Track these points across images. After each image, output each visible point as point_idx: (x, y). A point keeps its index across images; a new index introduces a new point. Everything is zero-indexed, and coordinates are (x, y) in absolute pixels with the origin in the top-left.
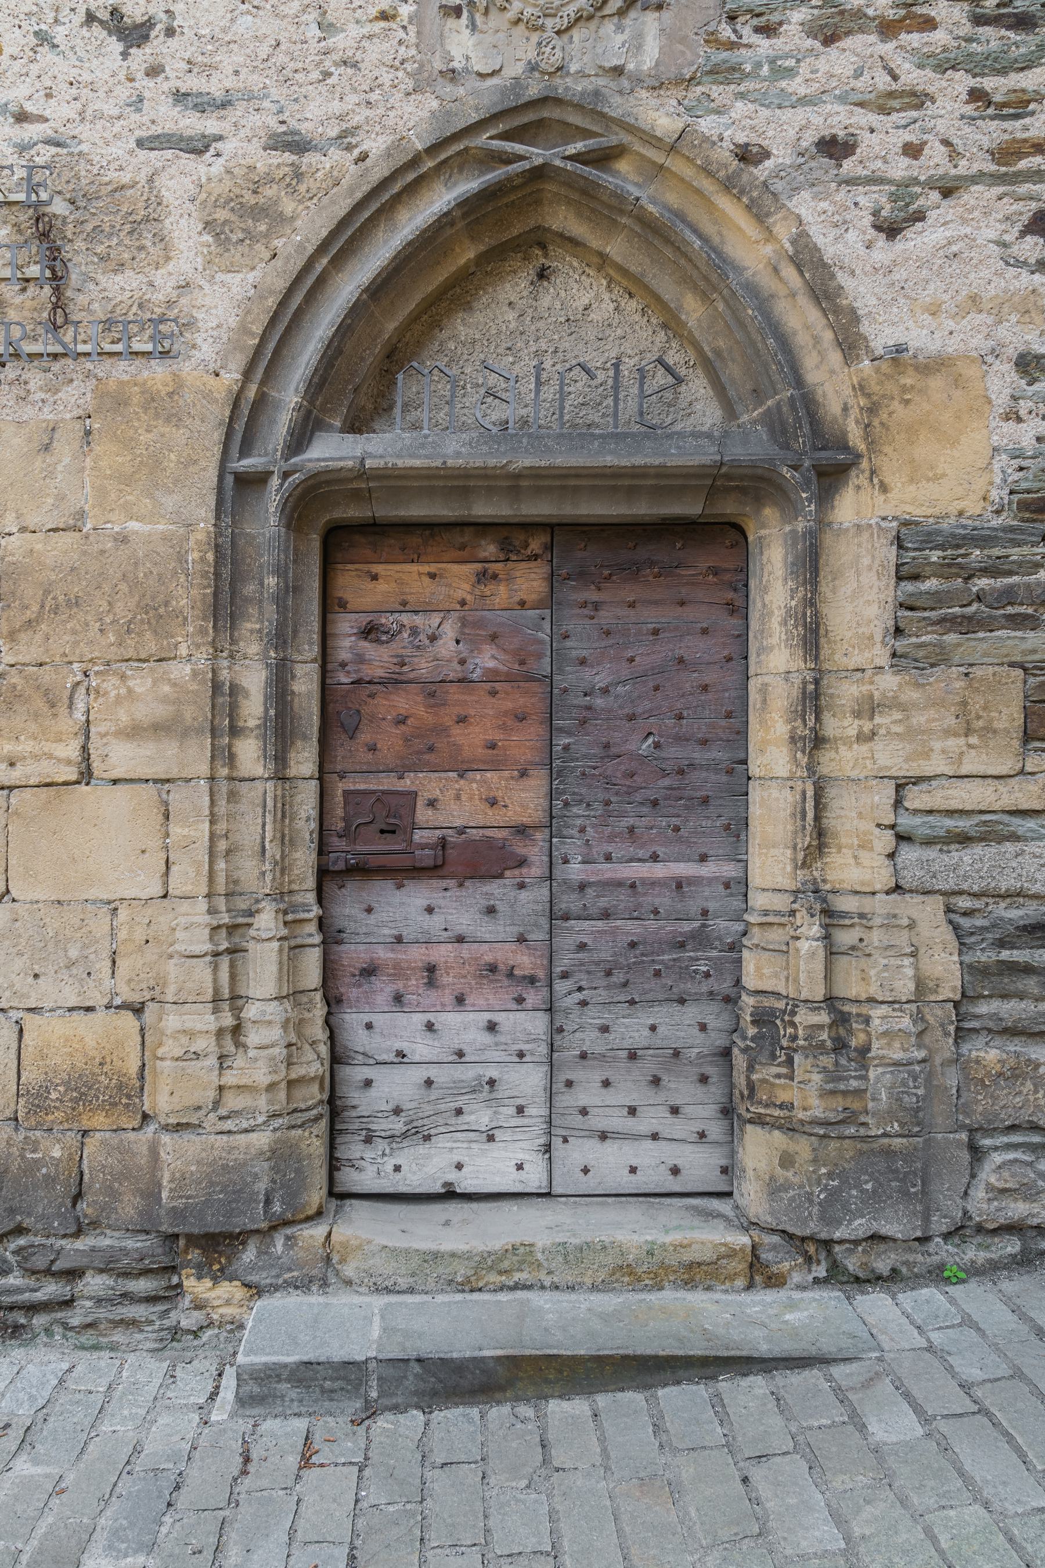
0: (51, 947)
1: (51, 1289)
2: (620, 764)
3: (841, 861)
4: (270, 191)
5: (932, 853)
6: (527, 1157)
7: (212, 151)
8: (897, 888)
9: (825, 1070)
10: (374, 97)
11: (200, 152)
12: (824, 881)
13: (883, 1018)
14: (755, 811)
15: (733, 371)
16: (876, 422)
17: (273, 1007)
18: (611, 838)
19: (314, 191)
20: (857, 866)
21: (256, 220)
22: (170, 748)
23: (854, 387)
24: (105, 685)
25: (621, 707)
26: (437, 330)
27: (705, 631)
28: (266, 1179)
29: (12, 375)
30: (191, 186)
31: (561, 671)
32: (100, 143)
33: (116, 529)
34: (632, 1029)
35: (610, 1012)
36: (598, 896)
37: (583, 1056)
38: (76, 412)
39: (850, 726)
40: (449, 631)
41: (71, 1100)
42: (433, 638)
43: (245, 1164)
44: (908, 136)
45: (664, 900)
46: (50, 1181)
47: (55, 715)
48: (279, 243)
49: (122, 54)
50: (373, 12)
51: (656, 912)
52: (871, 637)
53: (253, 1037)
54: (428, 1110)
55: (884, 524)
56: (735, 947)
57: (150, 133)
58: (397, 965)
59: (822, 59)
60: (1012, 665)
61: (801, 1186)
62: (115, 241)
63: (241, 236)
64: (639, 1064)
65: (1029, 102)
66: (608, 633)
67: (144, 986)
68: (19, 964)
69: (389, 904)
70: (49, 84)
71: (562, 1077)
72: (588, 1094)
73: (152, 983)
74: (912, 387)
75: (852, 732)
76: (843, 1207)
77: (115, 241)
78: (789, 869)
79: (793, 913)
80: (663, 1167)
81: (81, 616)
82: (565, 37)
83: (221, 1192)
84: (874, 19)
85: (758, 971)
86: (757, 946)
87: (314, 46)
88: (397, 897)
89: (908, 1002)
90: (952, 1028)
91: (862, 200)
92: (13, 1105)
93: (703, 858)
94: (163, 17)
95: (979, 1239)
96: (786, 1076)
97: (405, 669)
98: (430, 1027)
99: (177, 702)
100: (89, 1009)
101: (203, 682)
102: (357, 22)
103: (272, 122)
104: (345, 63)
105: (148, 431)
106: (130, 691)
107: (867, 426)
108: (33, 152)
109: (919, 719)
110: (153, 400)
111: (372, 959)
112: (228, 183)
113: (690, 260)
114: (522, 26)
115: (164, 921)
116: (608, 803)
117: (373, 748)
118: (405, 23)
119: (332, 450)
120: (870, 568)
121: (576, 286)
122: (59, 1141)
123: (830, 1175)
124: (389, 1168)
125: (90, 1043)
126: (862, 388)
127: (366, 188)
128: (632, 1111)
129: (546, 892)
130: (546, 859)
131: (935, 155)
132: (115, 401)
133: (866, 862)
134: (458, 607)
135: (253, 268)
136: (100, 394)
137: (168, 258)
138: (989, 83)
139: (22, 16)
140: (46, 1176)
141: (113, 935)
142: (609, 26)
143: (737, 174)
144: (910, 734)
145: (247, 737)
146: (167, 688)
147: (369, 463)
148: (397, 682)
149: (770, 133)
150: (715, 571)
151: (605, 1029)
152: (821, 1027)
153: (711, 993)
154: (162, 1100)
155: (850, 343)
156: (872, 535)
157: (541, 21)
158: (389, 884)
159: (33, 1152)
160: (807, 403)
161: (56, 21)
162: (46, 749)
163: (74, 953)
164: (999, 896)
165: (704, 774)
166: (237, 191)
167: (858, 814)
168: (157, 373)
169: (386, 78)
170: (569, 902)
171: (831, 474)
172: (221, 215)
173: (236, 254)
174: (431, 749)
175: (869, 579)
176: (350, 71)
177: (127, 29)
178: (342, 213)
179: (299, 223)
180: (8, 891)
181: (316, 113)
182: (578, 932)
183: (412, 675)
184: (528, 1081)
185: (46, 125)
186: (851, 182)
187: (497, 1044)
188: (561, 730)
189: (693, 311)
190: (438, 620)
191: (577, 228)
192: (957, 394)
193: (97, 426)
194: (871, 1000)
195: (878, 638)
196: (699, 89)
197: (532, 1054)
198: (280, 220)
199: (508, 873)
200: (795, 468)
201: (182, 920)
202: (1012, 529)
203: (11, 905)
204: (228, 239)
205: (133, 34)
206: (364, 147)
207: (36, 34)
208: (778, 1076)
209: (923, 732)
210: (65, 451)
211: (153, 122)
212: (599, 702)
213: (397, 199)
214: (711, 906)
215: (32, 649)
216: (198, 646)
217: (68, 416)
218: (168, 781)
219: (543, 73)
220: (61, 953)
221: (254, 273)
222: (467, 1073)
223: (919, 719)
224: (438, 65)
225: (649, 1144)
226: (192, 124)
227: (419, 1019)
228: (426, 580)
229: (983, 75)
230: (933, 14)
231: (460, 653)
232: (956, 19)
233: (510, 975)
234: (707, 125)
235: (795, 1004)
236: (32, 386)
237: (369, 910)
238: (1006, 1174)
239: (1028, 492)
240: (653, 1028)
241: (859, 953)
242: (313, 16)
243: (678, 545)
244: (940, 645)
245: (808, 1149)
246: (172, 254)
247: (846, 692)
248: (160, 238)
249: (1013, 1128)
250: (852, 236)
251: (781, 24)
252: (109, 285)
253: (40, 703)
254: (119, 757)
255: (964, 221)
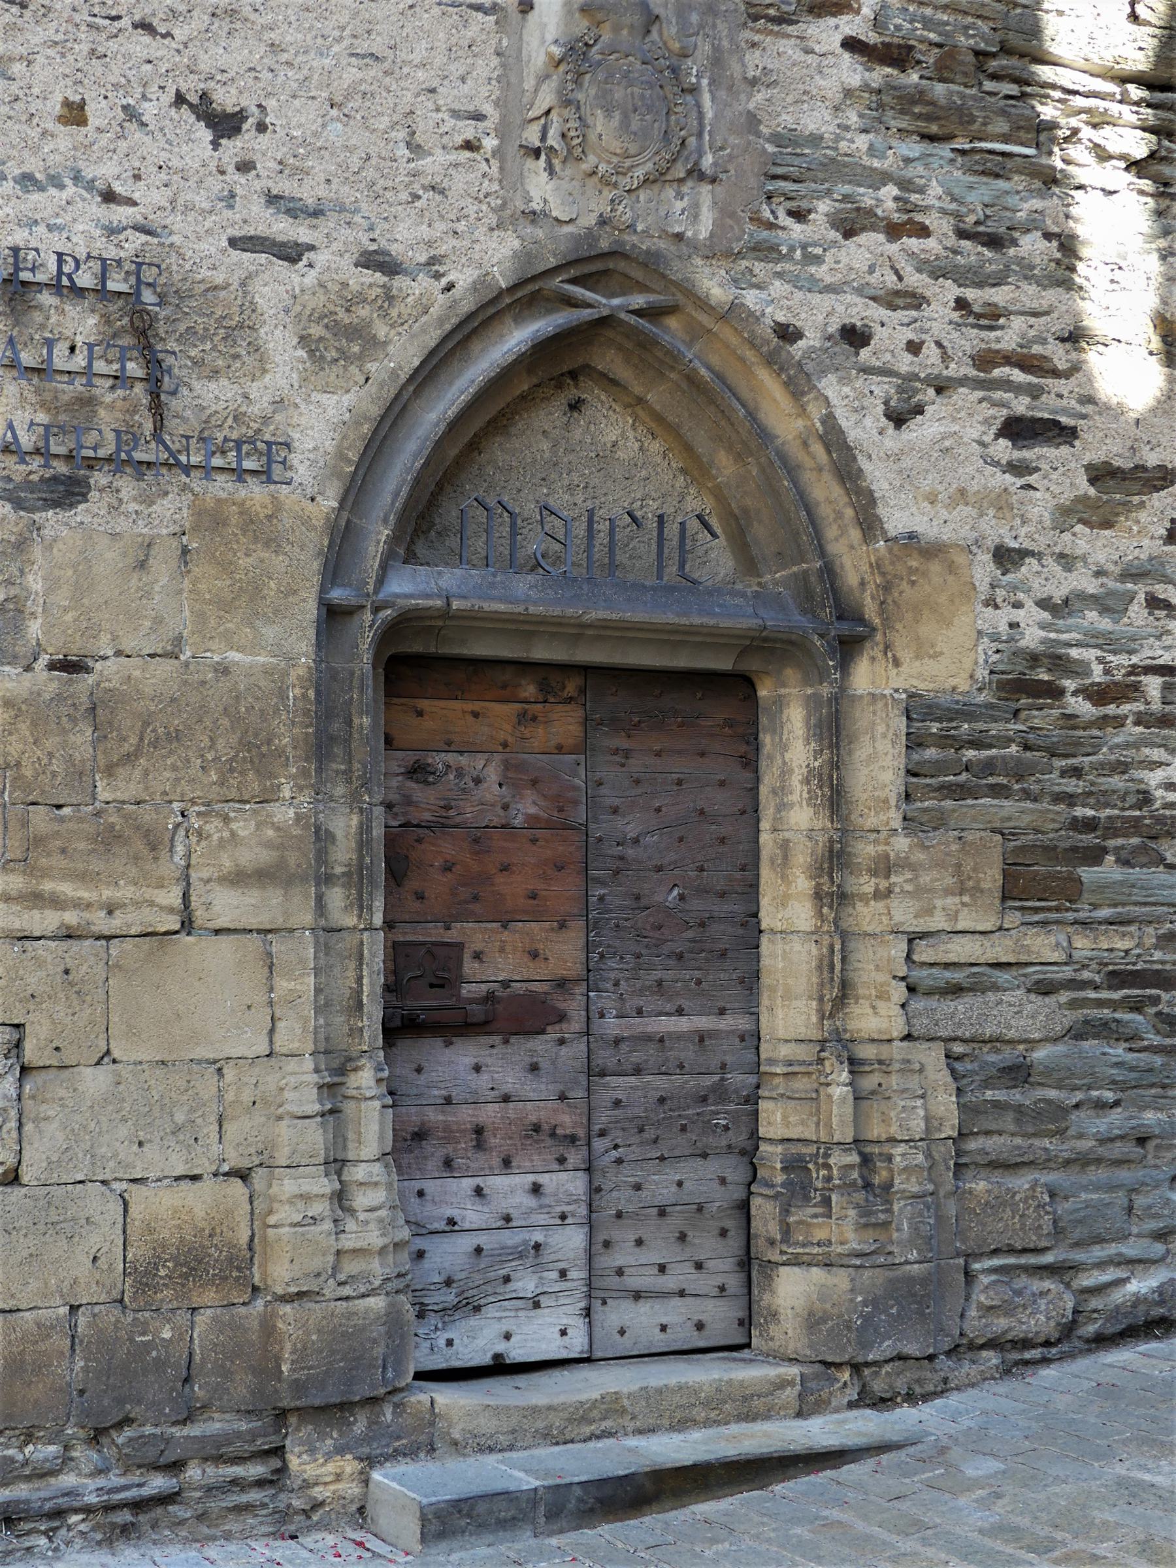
0: (156, 1112)
1: (158, 1483)
2: (648, 916)
3: (859, 1011)
4: (363, 312)
5: (933, 1002)
6: (571, 1322)
7: (305, 261)
8: (908, 1037)
9: (858, 1206)
10: (461, 227)
11: (294, 260)
12: (845, 1030)
13: (903, 1155)
14: (765, 962)
15: (759, 531)
16: (889, 601)
17: (377, 1168)
18: (641, 992)
19: (406, 317)
20: (876, 1017)
21: (350, 340)
22: (275, 896)
23: (871, 565)
24: (207, 827)
25: (650, 858)
26: (476, 453)
27: (722, 783)
28: (383, 1343)
29: (104, 481)
30: (286, 296)
31: (596, 820)
32: (193, 237)
33: (217, 658)
34: (661, 1185)
35: (642, 1169)
36: (630, 1051)
37: (619, 1215)
38: (171, 529)
39: (867, 884)
40: (493, 774)
41: (180, 1276)
42: (478, 781)
43: (363, 1329)
44: (911, 336)
45: (687, 1053)
46: (160, 1365)
47: (156, 859)
48: (372, 367)
49: (212, 142)
50: (459, 140)
51: (681, 1066)
52: (886, 801)
53: (362, 1200)
54: (478, 1279)
55: (896, 695)
56: (752, 1099)
57: (243, 233)
58: (447, 1128)
59: (843, 251)
60: (993, 831)
61: (840, 1316)
62: (208, 346)
63: (334, 354)
64: (669, 1220)
65: (1000, 316)
66: (637, 782)
67: (252, 1150)
68: (123, 1131)
69: (440, 1063)
70: (137, 164)
71: (601, 1237)
72: (625, 1256)
73: (261, 1146)
74: (917, 569)
75: (869, 889)
76: (875, 1330)
77: (208, 346)
78: (814, 1019)
79: (820, 1061)
80: (689, 1323)
81: (182, 752)
82: (633, 196)
83: (341, 1360)
84: (882, 219)
85: (777, 1120)
86: (782, 1095)
87: (404, 167)
88: (449, 1054)
89: (921, 1140)
90: (952, 1163)
91: (877, 391)
92: (119, 1285)
93: (722, 1012)
94: (255, 109)
95: (969, 1355)
96: (823, 1215)
97: (452, 813)
98: (479, 1191)
99: (281, 847)
100: (195, 1178)
101: (306, 827)
102: (444, 148)
103: (364, 238)
104: (433, 188)
105: (247, 555)
106: (233, 834)
107: (882, 603)
108: (122, 237)
109: (925, 879)
110: (252, 522)
111: (423, 1123)
112: (321, 298)
113: (732, 425)
114: (595, 179)
115: (271, 1081)
116: (639, 956)
117: (420, 897)
118: (488, 156)
119: (409, 586)
120: (884, 736)
121: (604, 421)
122: (169, 1321)
123: (865, 1303)
124: (442, 1342)
125: (199, 1212)
126: (878, 566)
127: (454, 321)
128: (662, 1268)
129: (583, 1047)
130: (584, 1013)
131: (931, 352)
132: (211, 519)
133: (883, 1012)
134: (500, 749)
135: (348, 391)
136: (199, 513)
137: (264, 371)
138: (971, 294)
139: (109, 87)
140: (157, 1360)
141: (220, 1098)
142: (670, 192)
143: (778, 350)
144: (919, 892)
145: (334, 885)
146: (270, 833)
147: (456, 604)
148: (444, 826)
149: (803, 316)
150: (730, 723)
151: (638, 1187)
152: (851, 1167)
153: (729, 1146)
154: (281, 1273)
155: (869, 525)
156: (886, 705)
157: (614, 178)
158: (439, 1042)
159: (143, 1334)
160: (829, 572)
161: (144, 97)
162: (147, 896)
163: (180, 1118)
164: (984, 1042)
165: (722, 927)
166: (331, 307)
167: (878, 963)
168: (255, 493)
169: (471, 210)
170: (606, 1057)
171: (848, 648)
172: (316, 331)
173: (331, 374)
174: (476, 898)
175: (883, 745)
176: (438, 198)
177: (216, 116)
178: (433, 344)
179: (391, 349)
180: (108, 1052)
181: (405, 237)
182: (614, 1088)
183: (458, 819)
184: (570, 1242)
185: (135, 209)
186: (867, 370)
187: (541, 1207)
188: (596, 880)
189: (725, 466)
190: (483, 762)
191: (622, 371)
192: (950, 578)
193: (195, 545)
194: (892, 1140)
195: (893, 802)
196: (745, 263)
197: (573, 1215)
198: (373, 344)
199: (549, 1029)
200: (821, 636)
201: (292, 1080)
202: (990, 706)
203: (112, 1067)
204: (322, 357)
205: (225, 125)
206: (451, 277)
207: (125, 108)
208: (815, 1216)
209: (929, 891)
210: (162, 569)
211: (245, 222)
212: (630, 852)
213: (475, 331)
214: (729, 1059)
215: (132, 786)
216: (301, 789)
217: (165, 532)
218: (270, 931)
219: (615, 228)
220: (167, 1119)
221: (348, 396)
222: (510, 1238)
223: (925, 879)
224: (520, 205)
225: (676, 1301)
226: (283, 228)
227: (468, 1184)
228: (470, 718)
229: (966, 286)
230: (927, 222)
231: (504, 797)
232: (945, 231)
233: (553, 1135)
234: (751, 298)
235: (830, 1145)
236: (124, 494)
237: (419, 1070)
238: (992, 1293)
239: (1003, 673)
240: (680, 1184)
241: (879, 1097)
242: (401, 135)
243: (699, 695)
244: (941, 810)
245: (847, 1280)
246: (268, 366)
247: (865, 850)
248: (255, 348)
249: (995, 1252)
250: (868, 421)
251: (809, 211)
252: (203, 393)
253: (140, 845)
254: (225, 905)
255: (954, 420)
